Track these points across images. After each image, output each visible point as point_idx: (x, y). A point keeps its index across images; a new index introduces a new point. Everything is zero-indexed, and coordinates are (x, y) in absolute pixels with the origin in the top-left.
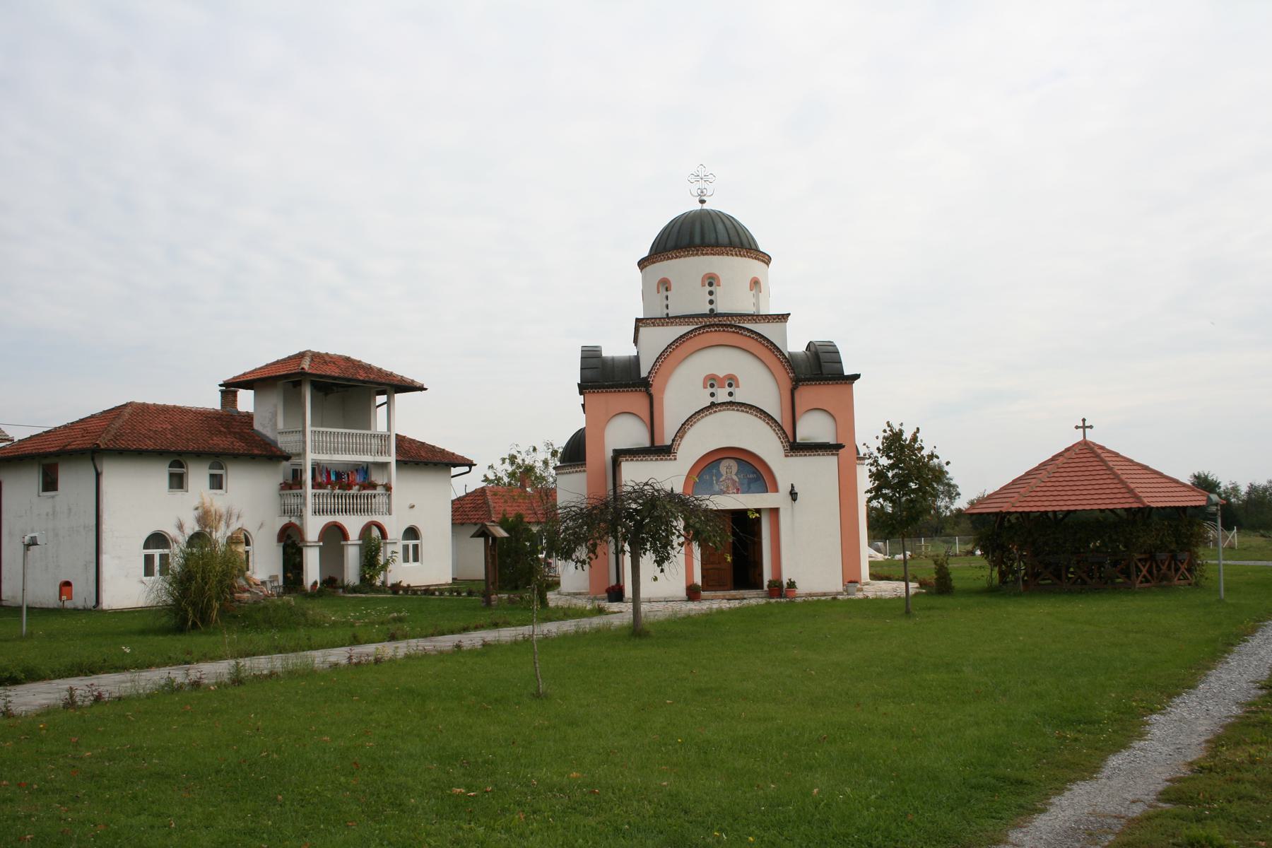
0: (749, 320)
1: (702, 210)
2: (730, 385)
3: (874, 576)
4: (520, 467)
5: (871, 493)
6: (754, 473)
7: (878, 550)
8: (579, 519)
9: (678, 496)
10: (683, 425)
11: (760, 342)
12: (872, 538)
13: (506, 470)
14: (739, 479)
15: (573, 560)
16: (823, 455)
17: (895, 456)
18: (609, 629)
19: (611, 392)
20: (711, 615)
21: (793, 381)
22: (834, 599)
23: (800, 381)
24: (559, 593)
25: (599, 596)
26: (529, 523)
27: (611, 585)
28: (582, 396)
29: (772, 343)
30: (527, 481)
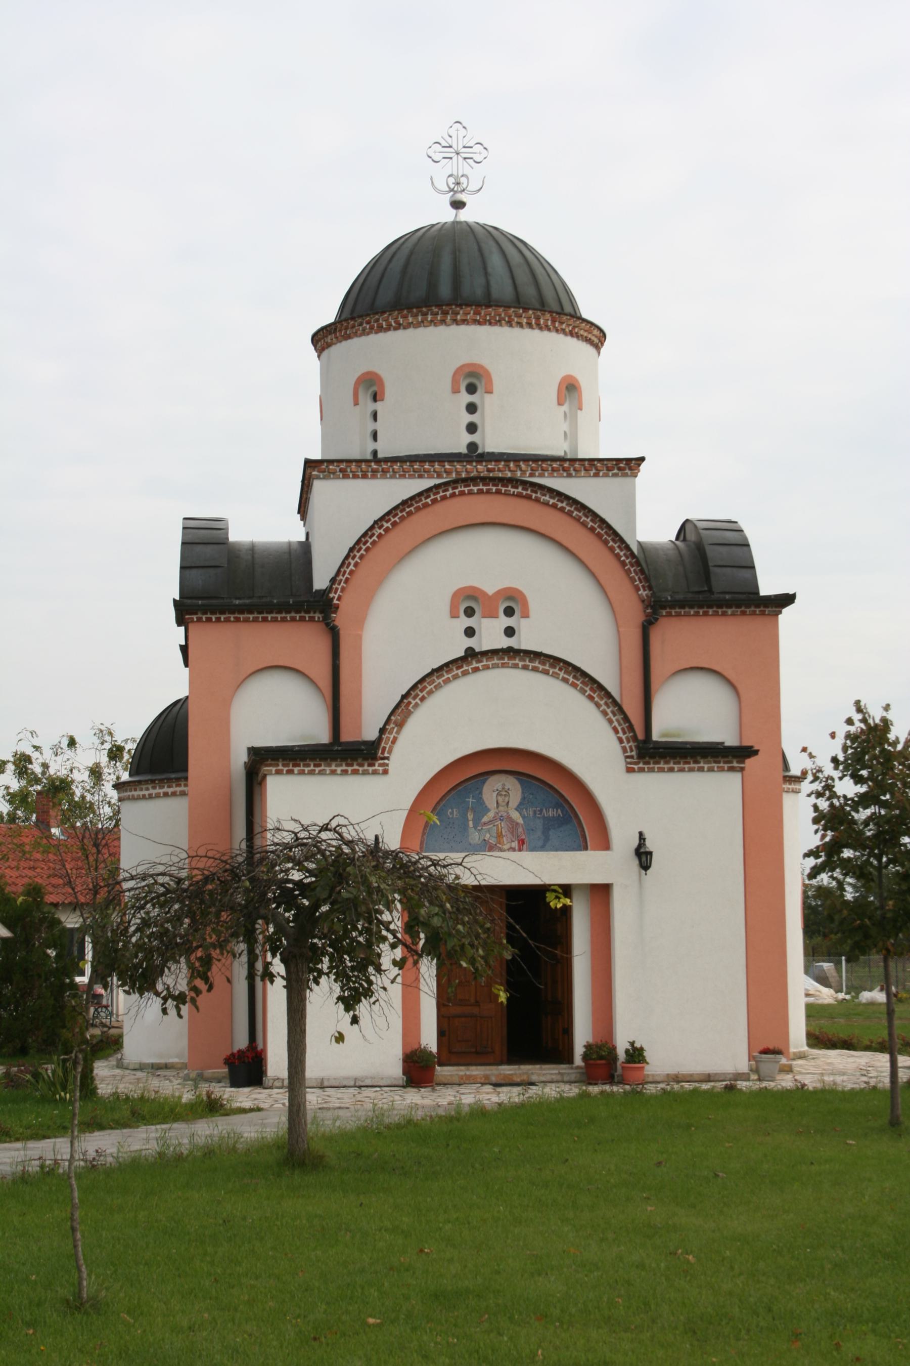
0: (553, 470)
1: (455, 223)
2: (509, 612)
3: (817, 1038)
4: (37, 781)
5: (817, 857)
6: (557, 806)
7: (823, 980)
8: (174, 901)
9: (394, 855)
10: (404, 697)
11: (578, 519)
12: (812, 953)
13: (7, 788)
14: (524, 817)
15: (157, 994)
16: (711, 770)
17: (871, 778)
18: (234, 1149)
19: (246, 620)
20: (458, 1120)
21: (646, 608)
22: (730, 1088)
23: (664, 608)
24: (120, 1065)
25: (209, 1073)
26: (56, 905)
27: (235, 1050)
28: (183, 628)
29: (603, 521)
30: (52, 813)
